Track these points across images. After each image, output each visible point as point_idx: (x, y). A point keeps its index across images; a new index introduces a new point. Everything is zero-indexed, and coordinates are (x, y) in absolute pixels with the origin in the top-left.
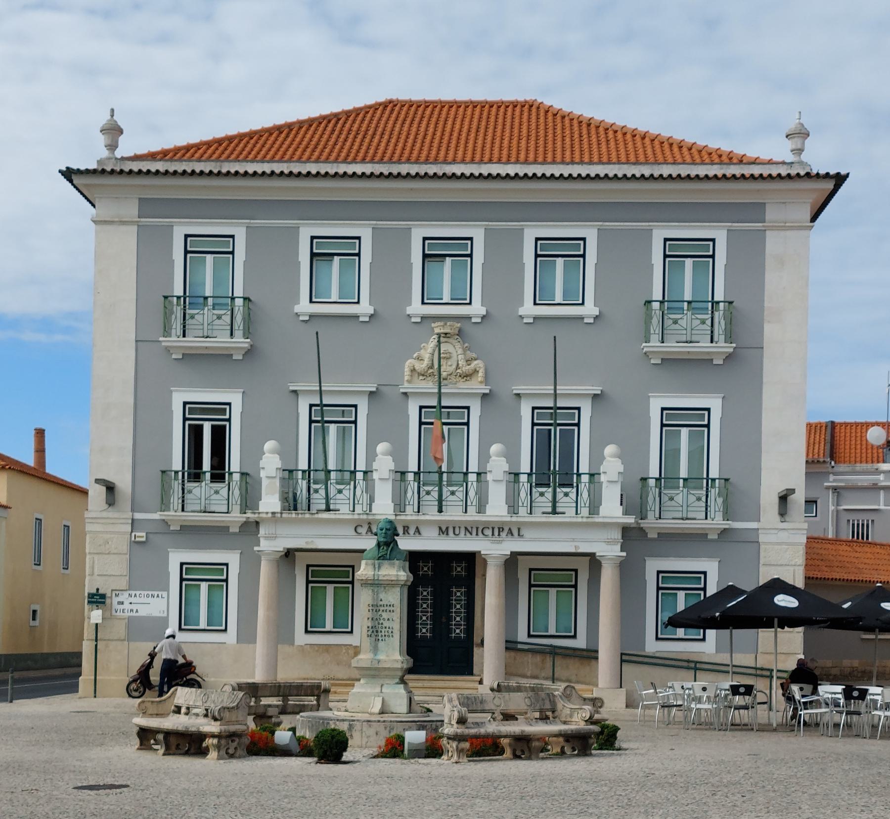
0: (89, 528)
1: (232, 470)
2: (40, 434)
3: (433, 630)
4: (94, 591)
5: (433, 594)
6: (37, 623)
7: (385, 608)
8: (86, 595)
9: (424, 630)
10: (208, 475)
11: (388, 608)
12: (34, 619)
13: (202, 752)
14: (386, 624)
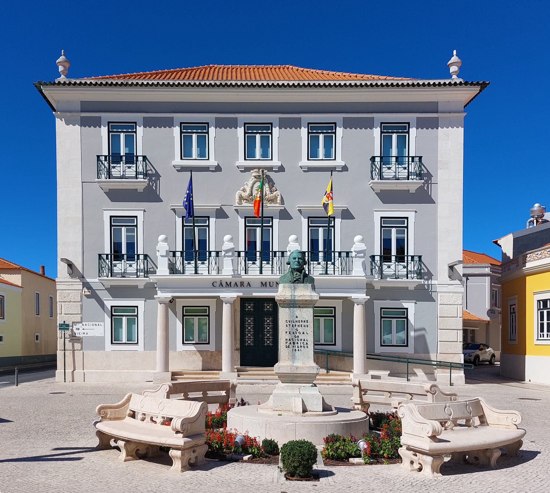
0: (58, 287)
1: (139, 253)
2: (43, 267)
3: (254, 342)
4: (63, 323)
5: (254, 321)
6: (38, 341)
7: (301, 323)
8: (58, 325)
9: (249, 342)
10: (125, 257)
11: (303, 324)
12: (37, 340)
13: (169, 462)
14: (301, 337)
